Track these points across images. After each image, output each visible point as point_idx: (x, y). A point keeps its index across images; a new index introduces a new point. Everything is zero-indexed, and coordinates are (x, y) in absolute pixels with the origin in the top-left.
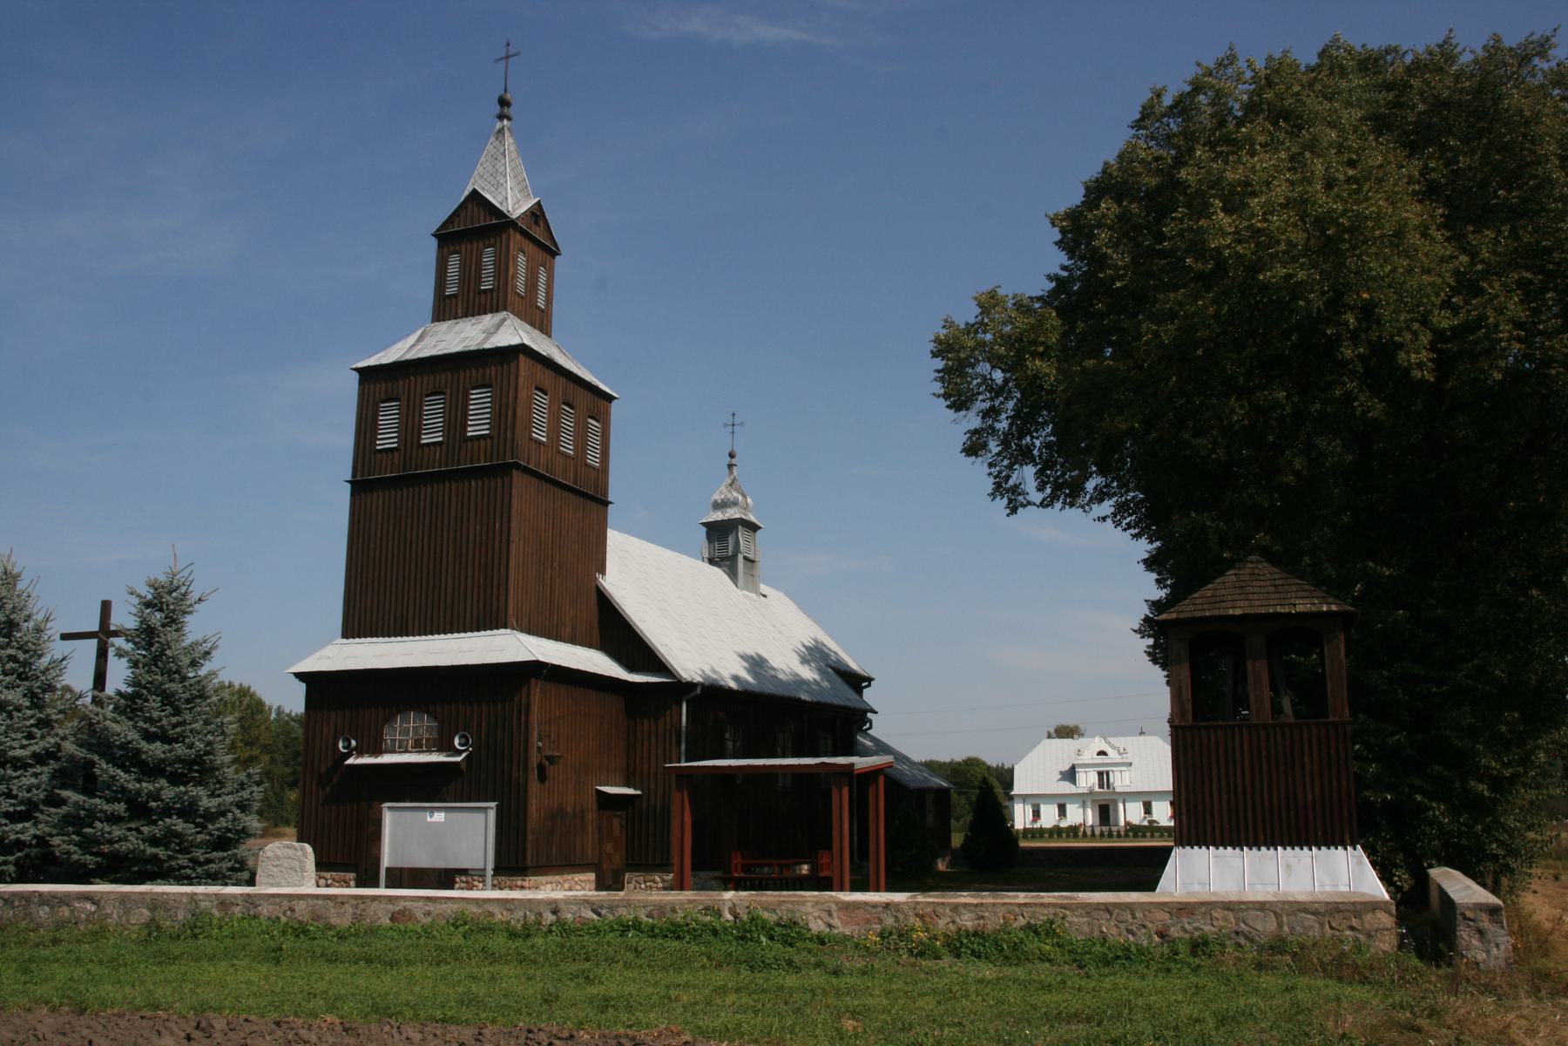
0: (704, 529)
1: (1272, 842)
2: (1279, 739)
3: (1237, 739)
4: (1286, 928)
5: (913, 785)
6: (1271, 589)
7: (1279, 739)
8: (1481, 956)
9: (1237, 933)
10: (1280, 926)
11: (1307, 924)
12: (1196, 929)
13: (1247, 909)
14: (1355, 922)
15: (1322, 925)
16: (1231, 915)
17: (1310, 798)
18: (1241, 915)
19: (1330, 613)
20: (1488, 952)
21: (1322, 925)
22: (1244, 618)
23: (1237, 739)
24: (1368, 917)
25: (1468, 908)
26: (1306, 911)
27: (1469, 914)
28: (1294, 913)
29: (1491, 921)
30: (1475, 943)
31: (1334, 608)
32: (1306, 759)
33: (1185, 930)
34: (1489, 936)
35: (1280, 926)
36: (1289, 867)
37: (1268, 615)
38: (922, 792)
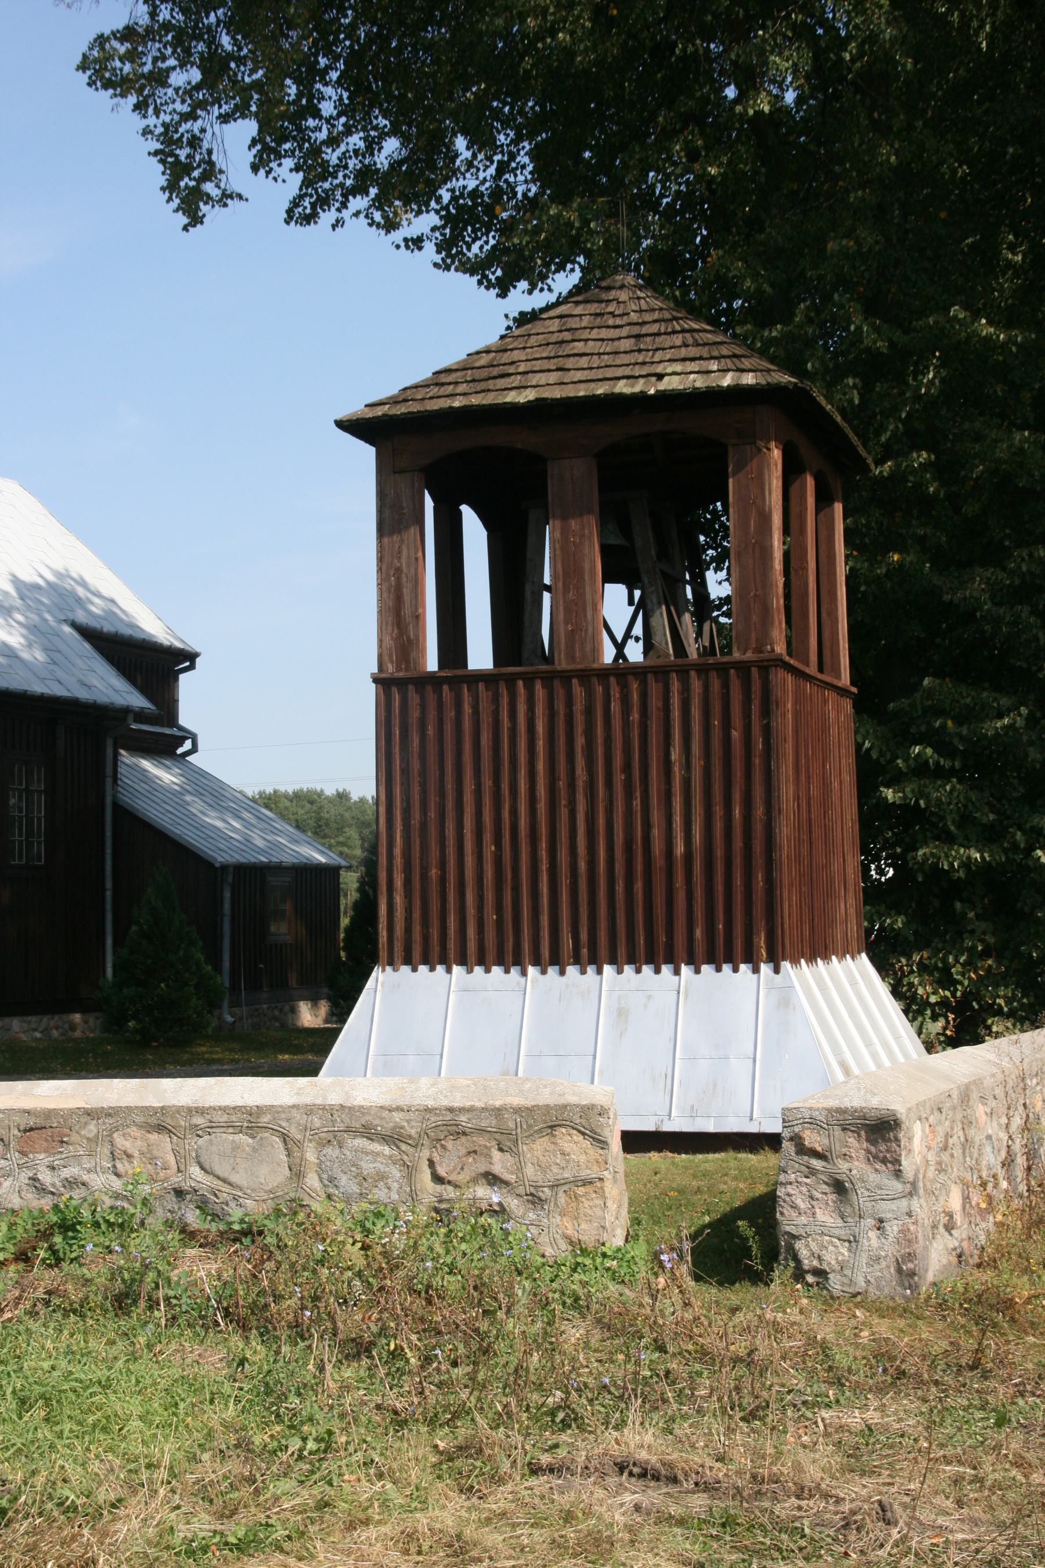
0: (363, 456)
1: (591, 957)
2: (615, 707)
3: (522, 708)
4: (312, 1181)
5: (221, 858)
6: (626, 344)
7: (615, 707)
8: (834, 1254)
9: (179, 1193)
10: (297, 1173)
11: (368, 1167)
12: (71, 1183)
13: (211, 1127)
14: (500, 1163)
15: (410, 1171)
16: (164, 1145)
17: (679, 849)
18: (192, 1143)
19: (737, 392)
20: (853, 1241)
21: (410, 1171)
22: (540, 409)
23: (522, 708)
24: (536, 1149)
25: (813, 1122)
26: (368, 1132)
27: (813, 1139)
28: (333, 1139)
29: (873, 1158)
30: (826, 1217)
31: (749, 379)
32: (675, 755)
33: (41, 1189)
34: (861, 1198)
35: (297, 1173)
36: (621, 1014)
37: (592, 401)
38: (254, 878)
